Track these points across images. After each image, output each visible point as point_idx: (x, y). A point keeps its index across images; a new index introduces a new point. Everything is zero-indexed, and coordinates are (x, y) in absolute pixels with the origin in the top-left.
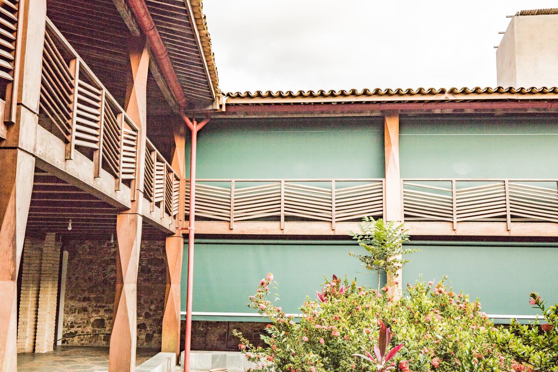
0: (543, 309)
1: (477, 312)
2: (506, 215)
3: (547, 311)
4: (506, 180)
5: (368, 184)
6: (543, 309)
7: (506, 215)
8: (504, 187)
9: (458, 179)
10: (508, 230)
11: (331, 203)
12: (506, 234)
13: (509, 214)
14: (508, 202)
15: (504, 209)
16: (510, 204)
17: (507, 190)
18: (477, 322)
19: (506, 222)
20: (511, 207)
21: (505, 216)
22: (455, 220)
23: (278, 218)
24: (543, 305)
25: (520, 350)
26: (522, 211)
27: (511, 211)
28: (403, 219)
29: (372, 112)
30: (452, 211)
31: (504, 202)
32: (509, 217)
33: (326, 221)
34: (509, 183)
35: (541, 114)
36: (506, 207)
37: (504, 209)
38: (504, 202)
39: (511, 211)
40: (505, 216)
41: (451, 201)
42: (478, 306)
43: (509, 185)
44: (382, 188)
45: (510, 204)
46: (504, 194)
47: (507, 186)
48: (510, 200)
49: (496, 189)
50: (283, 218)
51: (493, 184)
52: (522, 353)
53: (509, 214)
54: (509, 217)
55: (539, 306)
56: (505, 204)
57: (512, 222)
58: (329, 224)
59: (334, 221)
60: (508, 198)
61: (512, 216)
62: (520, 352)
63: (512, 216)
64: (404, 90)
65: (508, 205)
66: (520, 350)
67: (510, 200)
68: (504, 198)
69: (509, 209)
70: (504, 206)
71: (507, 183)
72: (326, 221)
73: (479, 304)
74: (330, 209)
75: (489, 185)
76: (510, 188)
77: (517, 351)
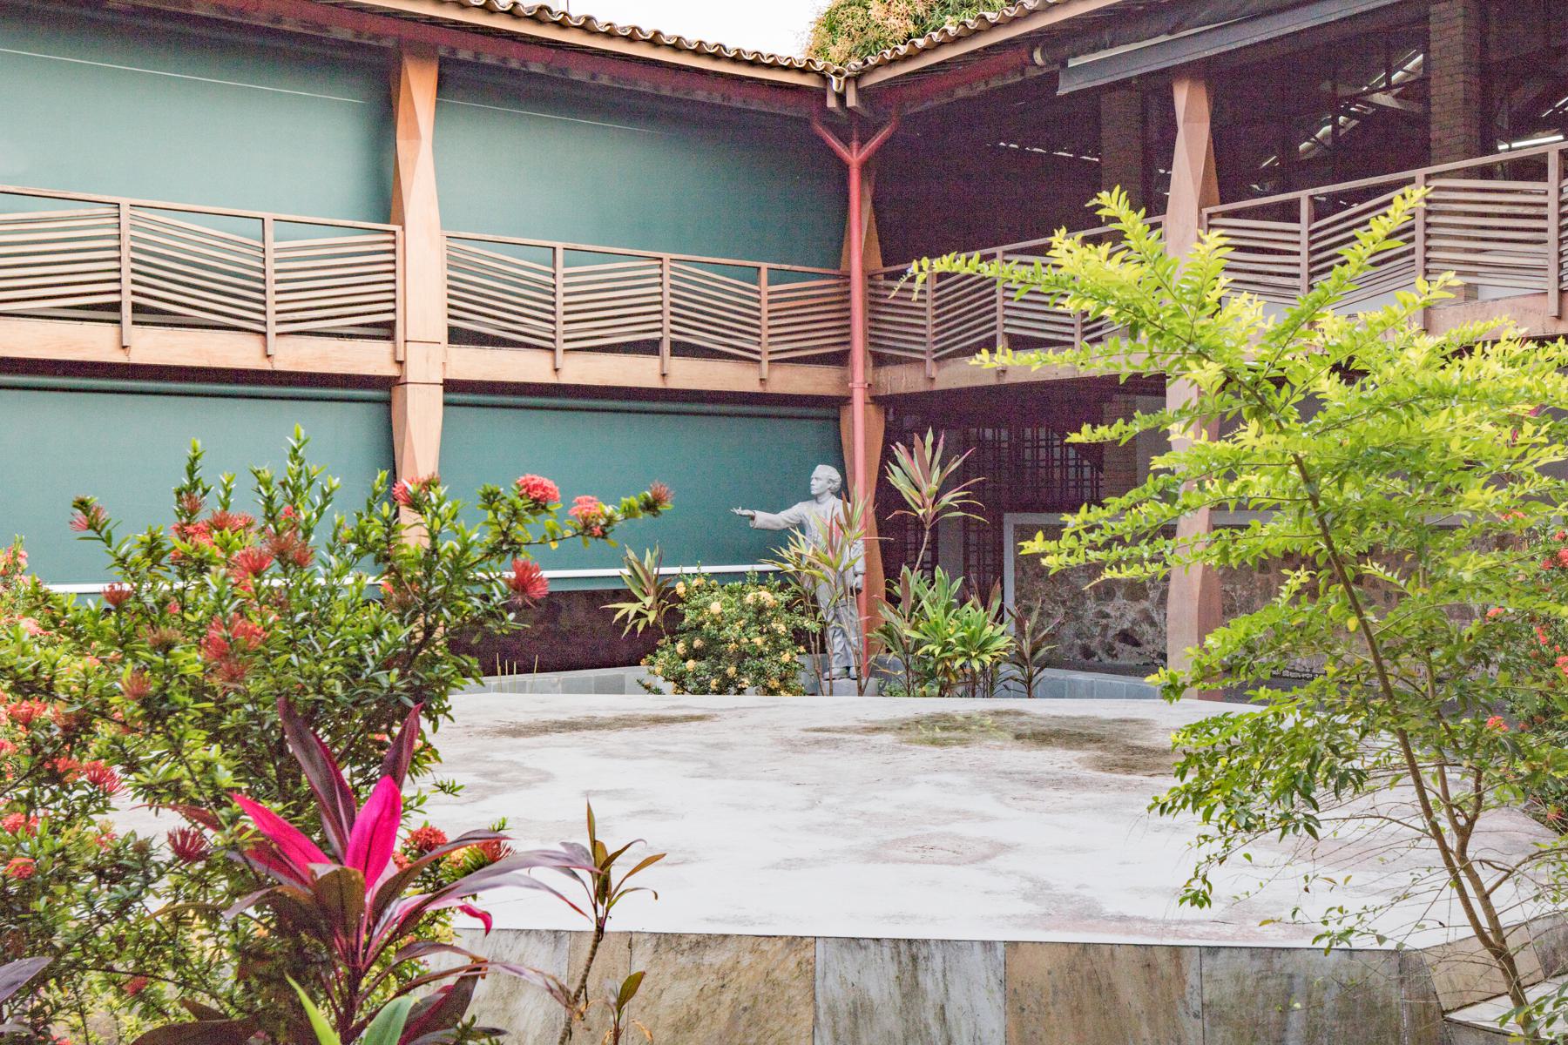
0: (108, 540)
1: (17, 577)
2: (120, 303)
3: (119, 547)
4: (125, 202)
5: (56, 209)
6: (108, 540)
7: (120, 303)
8: (116, 221)
9: (571, 245)
10: (124, 347)
11: (553, 304)
12: (119, 357)
13: (127, 300)
14: (127, 266)
15: (114, 287)
16: (133, 271)
17: (126, 232)
18: (14, 606)
19: (118, 322)
20: (134, 282)
21: (116, 307)
22: (272, 329)
23: (651, 348)
24: (109, 532)
25: (23, 660)
26: (165, 296)
27: (134, 293)
28: (443, 335)
29: (613, 79)
30: (264, 303)
31: (114, 265)
32: (127, 310)
33: (538, 347)
34: (132, 212)
35: (227, 23)
36: (119, 281)
37: (114, 287)
38: (114, 265)
39: (134, 293)
40: (116, 307)
41: (261, 276)
42: (19, 560)
43: (133, 217)
44: (393, 252)
45: (133, 271)
46: (114, 243)
47: (125, 221)
48: (133, 260)
49: (91, 224)
50: (666, 348)
51: (84, 210)
52: (30, 667)
53: (127, 300)
54: (127, 310)
55: (99, 533)
56: (119, 270)
57: (135, 323)
58: (547, 356)
59: (560, 346)
60: (126, 254)
61: (137, 308)
62: (24, 666)
63: (137, 308)
64: (601, 21)
65: (127, 276)
66: (23, 660)
67: (133, 260)
68: (115, 254)
69: (127, 287)
70: (115, 275)
71: (125, 210)
72: (538, 347)
73: (24, 553)
74: (551, 317)
75: (73, 213)
76: (133, 227)
77: (14, 663)
